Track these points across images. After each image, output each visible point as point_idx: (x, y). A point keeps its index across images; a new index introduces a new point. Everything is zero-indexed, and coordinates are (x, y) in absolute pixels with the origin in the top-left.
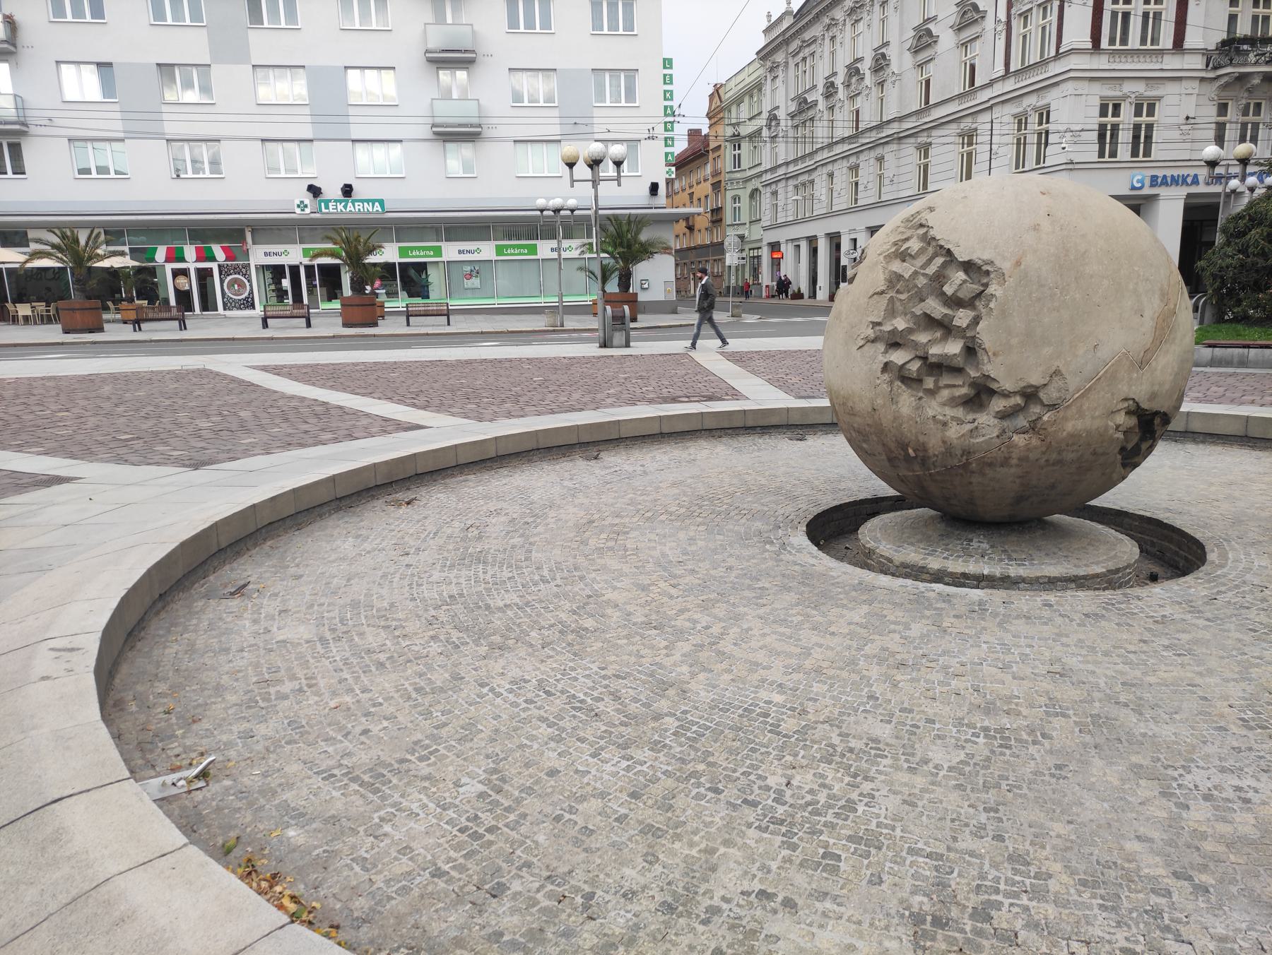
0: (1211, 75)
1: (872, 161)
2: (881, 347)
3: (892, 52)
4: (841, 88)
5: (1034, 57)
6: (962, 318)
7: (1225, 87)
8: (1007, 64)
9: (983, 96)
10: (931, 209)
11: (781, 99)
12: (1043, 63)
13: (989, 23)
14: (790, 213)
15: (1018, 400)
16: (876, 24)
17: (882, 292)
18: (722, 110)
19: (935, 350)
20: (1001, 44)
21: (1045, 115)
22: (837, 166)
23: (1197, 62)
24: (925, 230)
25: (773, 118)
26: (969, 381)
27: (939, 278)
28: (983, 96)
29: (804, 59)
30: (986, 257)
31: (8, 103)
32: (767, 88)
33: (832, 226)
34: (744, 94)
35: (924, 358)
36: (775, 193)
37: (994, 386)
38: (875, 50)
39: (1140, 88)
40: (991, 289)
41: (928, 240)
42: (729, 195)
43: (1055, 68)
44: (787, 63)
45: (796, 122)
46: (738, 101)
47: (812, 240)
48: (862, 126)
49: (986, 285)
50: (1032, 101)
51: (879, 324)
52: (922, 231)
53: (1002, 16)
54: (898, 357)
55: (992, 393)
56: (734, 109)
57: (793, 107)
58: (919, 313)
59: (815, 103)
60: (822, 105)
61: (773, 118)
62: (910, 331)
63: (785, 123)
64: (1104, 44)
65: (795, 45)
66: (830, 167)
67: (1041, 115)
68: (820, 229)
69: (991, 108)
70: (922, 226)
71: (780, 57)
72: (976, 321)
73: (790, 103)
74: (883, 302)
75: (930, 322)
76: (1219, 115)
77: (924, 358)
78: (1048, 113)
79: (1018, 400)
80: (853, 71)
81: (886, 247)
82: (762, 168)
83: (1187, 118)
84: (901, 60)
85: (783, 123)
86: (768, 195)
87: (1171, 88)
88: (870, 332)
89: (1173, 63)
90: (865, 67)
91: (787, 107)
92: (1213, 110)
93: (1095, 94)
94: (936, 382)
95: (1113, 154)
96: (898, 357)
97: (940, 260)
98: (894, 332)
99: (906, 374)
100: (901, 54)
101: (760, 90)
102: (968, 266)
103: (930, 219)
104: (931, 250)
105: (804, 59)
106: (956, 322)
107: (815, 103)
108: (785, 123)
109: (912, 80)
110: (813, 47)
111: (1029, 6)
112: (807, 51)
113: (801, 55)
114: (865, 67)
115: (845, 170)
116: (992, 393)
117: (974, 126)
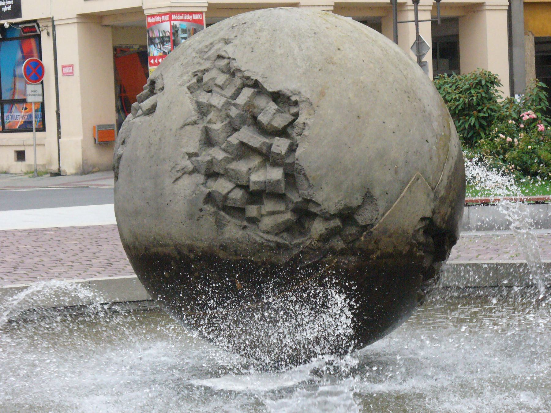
2: (199, 178)
6: (280, 145)
15: (337, 222)
19: (255, 177)
24: (226, 61)
26: (291, 206)
27: (249, 108)
31: (144, 395)
35: (245, 187)
37: (314, 209)
40: (301, 120)
49: (296, 115)
51: (196, 155)
54: (222, 186)
70: (219, 57)
72: (292, 149)
75: (245, 151)
77: (245, 187)
79: (337, 222)
88: (188, 164)
94: (259, 210)
99: (229, 203)
102: (277, 97)
104: (238, 82)
116: (313, 216)
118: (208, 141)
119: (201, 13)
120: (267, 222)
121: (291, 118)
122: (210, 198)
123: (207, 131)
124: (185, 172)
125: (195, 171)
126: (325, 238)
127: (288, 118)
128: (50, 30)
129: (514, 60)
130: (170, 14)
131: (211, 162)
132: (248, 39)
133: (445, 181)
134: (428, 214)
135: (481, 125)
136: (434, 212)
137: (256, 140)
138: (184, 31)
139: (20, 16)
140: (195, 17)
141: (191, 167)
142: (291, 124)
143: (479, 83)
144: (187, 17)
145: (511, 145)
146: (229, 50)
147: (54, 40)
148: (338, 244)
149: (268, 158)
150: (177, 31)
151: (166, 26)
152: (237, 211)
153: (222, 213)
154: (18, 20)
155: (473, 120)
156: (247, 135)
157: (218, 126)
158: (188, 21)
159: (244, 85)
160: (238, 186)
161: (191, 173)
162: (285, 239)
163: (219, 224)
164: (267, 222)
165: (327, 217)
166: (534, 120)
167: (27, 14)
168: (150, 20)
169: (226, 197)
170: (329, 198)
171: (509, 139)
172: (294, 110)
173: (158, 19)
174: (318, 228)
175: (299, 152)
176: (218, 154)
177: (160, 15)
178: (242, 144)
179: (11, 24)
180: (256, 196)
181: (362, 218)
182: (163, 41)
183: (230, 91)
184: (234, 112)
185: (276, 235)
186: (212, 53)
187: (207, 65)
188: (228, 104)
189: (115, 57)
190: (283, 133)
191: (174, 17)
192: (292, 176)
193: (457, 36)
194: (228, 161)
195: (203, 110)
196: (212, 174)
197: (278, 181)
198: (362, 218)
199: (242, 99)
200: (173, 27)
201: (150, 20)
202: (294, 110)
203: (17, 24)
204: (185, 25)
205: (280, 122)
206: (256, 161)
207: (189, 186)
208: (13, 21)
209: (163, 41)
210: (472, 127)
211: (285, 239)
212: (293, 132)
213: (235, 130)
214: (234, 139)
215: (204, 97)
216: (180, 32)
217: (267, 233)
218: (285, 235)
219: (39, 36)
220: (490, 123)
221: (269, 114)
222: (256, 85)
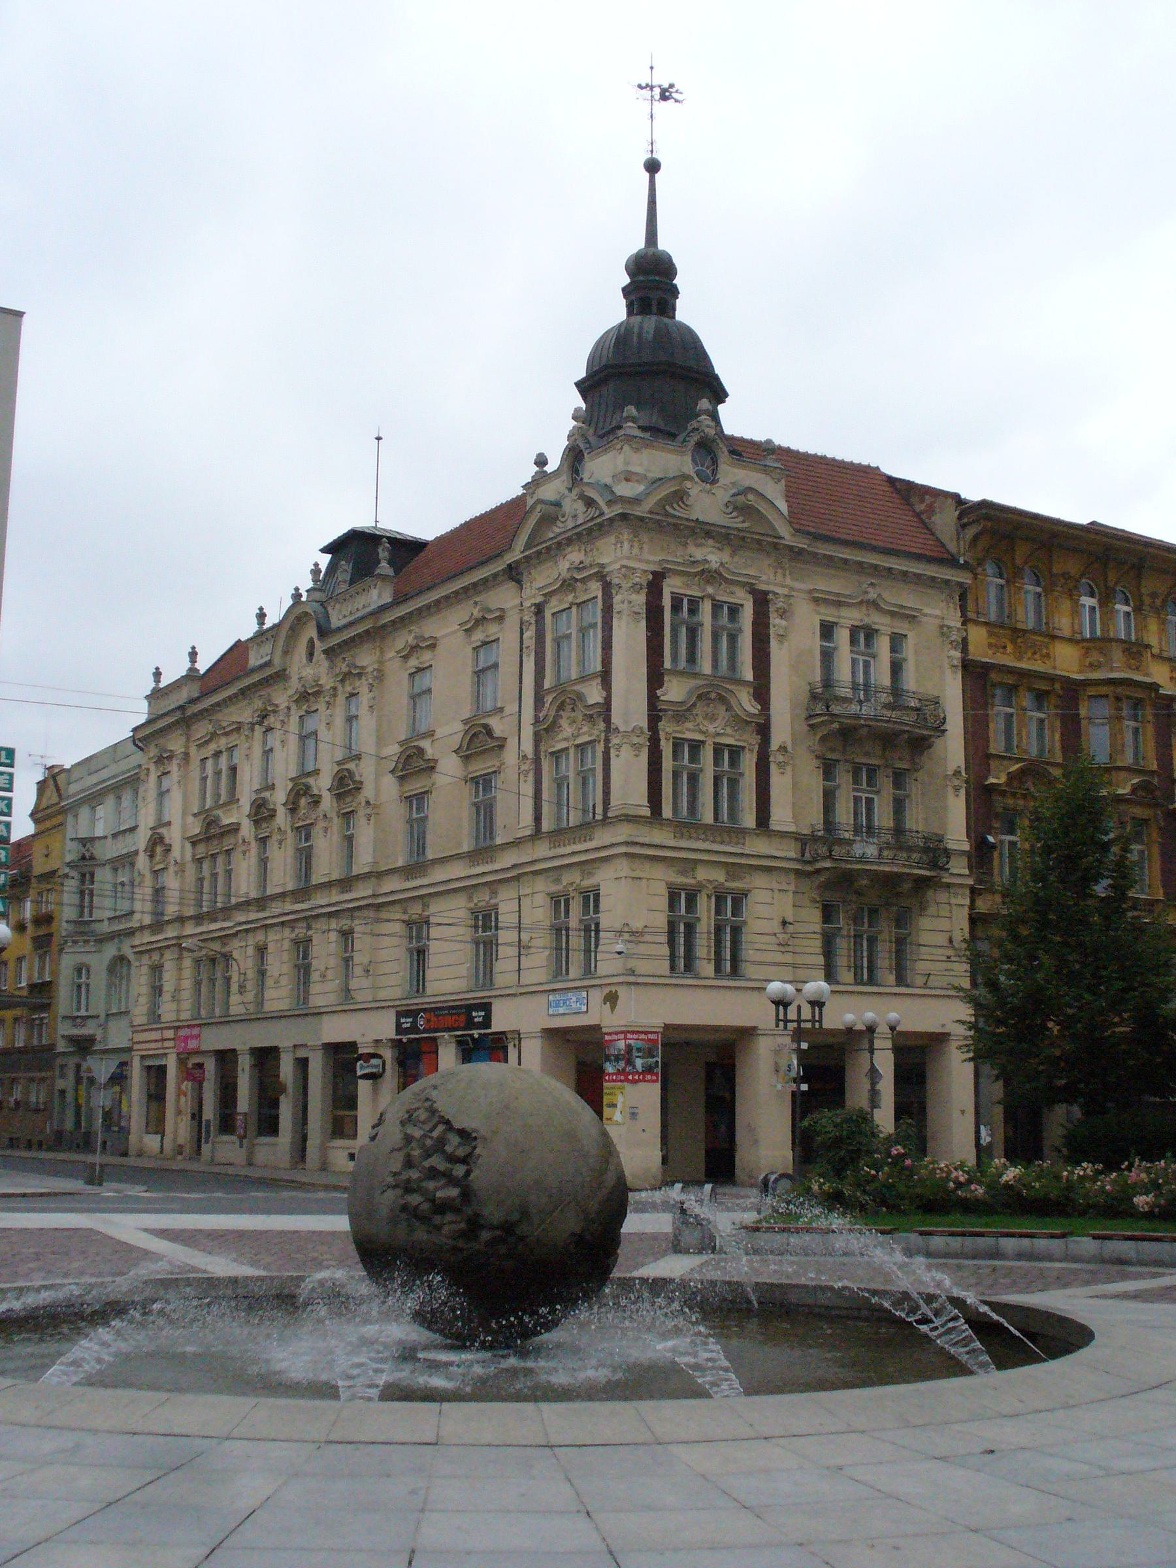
0: (809, 868)
1: (333, 936)
2: (399, 1192)
3: (366, 771)
4: (281, 812)
5: (574, 819)
6: (459, 1170)
8: (538, 818)
10: (435, 1087)
11: (174, 808)
13: (510, 756)
15: (498, 1233)
16: (339, 721)
17: (400, 1149)
18: (63, 811)
19: (439, 1194)
20: (528, 789)
22: (273, 936)
23: (789, 850)
25: (157, 842)
27: (442, 1141)
28: (507, 860)
29: (218, 754)
30: (473, 1126)
33: (262, 1036)
36: (157, 969)
38: (339, 763)
39: (719, 876)
40: (477, 1151)
41: (433, 1111)
42: (68, 962)
43: (603, 837)
45: (201, 850)
46: (93, 799)
47: (226, 1057)
48: (316, 879)
49: (475, 1148)
50: (573, 878)
52: (427, 1104)
53: (528, 747)
54: (415, 1199)
55: (482, 1227)
56: (84, 812)
57: (196, 829)
61: (157, 842)
62: (420, 1180)
64: (667, 812)
66: (260, 937)
68: (243, 1039)
69: (518, 878)
70: (427, 1099)
71: (175, 744)
74: (400, 1157)
75: (433, 1173)
76: (825, 922)
77: (433, 1201)
81: (401, 1114)
82: (134, 924)
83: (784, 923)
84: (381, 786)
85: (176, 853)
86: (145, 970)
87: (759, 881)
88: (390, 1180)
89: (760, 846)
91: (184, 827)
93: (659, 879)
97: (441, 1128)
100: (378, 776)
102: (463, 1133)
104: (435, 1120)
105: (218, 754)
107: (235, 829)
109: (395, 813)
110: (233, 739)
111: (563, 745)
112: (223, 742)
113: (213, 747)
114: (323, 784)
115: (287, 945)
116: (482, 1227)
117: (493, 901)
118: (409, 1163)
122: (405, 1208)
123: (408, 1155)
125: (396, 1186)
127: (467, 1149)
131: (408, 1181)
134: (578, 1229)
138: (639, 1050)
139: (490, 1027)
142: (470, 1155)
144: (643, 1036)
146: (434, 1094)
149: (451, 1180)
151: (621, 1044)
152: (424, 1219)
154: (489, 1031)
155: (842, 1153)
156: (436, 1161)
159: (439, 1122)
160: (427, 1200)
162: (461, 1243)
164: (446, 1230)
165: (492, 1228)
166: (903, 1155)
167: (496, 1027)
168: (607, 1038)
169: (416, 1207)
170: (492, 1213)
171: (873, 1172)
172: (474, 1144)
173: (615, 1037)
174: (485, 1235)
176: (414, 1174)
177: (616, 1033)
180: (441, 1207)
182: (617, 1058)
183: (427, 1127)
184: (429, 1142)
186: (423, 1096)
187: (417, 1105)
190: (464, 1160)
191: (629, 1036)
195: (408, 1139)
196: (408, 1188)
199: (435, 1134)
204: (640, 1044)
205: (461, 1152)
206: (442, 1182)
208: (482, 1031)
209: (617, 1058)
210: (842, 1159)
211: (461, 1243)
213: (429, 1156)
214: (426, 1164)
221: (453, 1144)
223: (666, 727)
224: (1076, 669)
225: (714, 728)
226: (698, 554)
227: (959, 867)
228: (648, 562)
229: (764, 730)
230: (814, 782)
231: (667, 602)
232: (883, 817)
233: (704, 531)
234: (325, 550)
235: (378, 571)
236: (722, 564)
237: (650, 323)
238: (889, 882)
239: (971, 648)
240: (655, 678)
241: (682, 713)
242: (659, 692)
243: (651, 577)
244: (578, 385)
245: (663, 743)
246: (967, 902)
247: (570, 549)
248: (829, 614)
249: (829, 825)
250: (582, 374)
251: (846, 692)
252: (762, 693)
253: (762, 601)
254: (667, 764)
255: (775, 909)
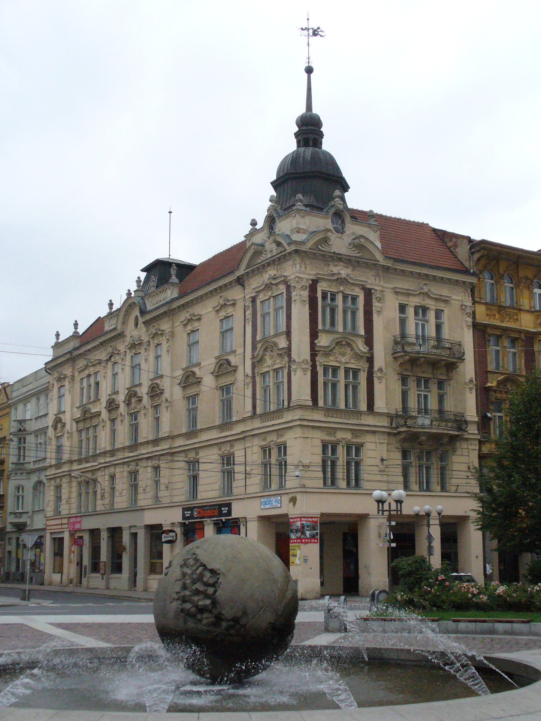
1: (149, 469)
2: (179, 602)
3: (165, 384)
4: (122, 406)
6: (211, 590)
7: (404, 440)
9: (239, 429)
10: (198, 547)
11: (67, 405)
12: (279, 412)
13: (240, 375)
14: (74, 506)
15: (232, 623)
17: (180, 580)
18: (10, 406)
19: (200, 603)
21: (282, 448)
22: (118, 469)
23: (384, 422)
27: (201, 575)
28: (239, 429)
29: (89, 376)
32: (54, 393)
33: (114, 522)
34: (32, 395)
39: (348, 436)
40: (219, 581)
41: (196, 560)
44: (73, 376)
45: (81, 425)
47: (94, 533)
49: (218, 579)
51: (179, 593)
54: (188, 606)
58: (194, 588)
59: (99, 414)
60: (105, 415)
61: (58, 421)
63: (70, 426)
64: (321, 403)
65: (81, 363)
66: (112, 470)
67: (280, 449)
68: (103, 523)
69: (244, 438)
70: (194, 554)
72: (215, 591)
73: (75, 410)
74: (180, 584)
75: (197, 592)
77: (197, 606)
78: (285, 448)
80: (132, 395)
85: (68, 427)
86: (52, 488)
88: (176, 596)
89: (369, 420)
90: (143, 391)
92: (399, 455)
95: (333, 483)
96: (188, 606)
97: (201, 569)
98: (184, 596)
100: (172, 386)
101: (47, 395)
102: (212, 571)
103: (198, 551)
104: (198, 564)
105: (89, 376)
106: (208, 592)
107: (99, 414)
108: (70, 426)
109: (181, 406)
110: (98, 368)
112: (92, 370)
113: (87, 372)
114: (143, 391)
115: (125, 474)
116: (222, 620)
118: (184, 587)
119: (317, 517)
120: (205, 621)
121: (216, 580)
122: (182, 610)
124: (174, 599)
126: (228, 628)
127: (215, 579)
128: (245, 523)
129: (482, 548)
130: (301, 518)
132: (205, 547)
133: (282, 609)
134: (273, 621)
135: (417, 582)
136: (275, 621)
137: (201, 588)
138: (308, 527)
140: (314, 519)
141: (176, 597)
142: (216, 582)
143: (417, 561)
144: (310, 520)
145: (430, 592)
147: (246, 527)
148: (233, 632)
149: (207, 596)
150: (304, 527)
151: (299, 524)
152: (193, 616)
153: (187, 617)
154: (230, 518)
156: (199, 586)
157: (188, 582)
158: (310, 521)
161: (177, 600)
163: (185, 622)
164: (205, 621)
167: (234, 515)
168: (291, 520)
170: (228, 612)
171: (429, 589)
172: (218, 577)
173: (295, 520)
174: (224, 624)
175: (217, 593)
176: (187, 593)
177: (296, 518)
178: (197, 589)
179: (226, 519)
180: (202, 610)
181: (243, 621)
185: (208, 626)
187: (189, 557)
188: (193, 573)
189: (277, 538)
190: (213, 585)
191: (302, 519)
192: (214, 603)
193: (456, 532)
194: (191, 596)
195: (184, 575)
197: (208, 605)
198: (243, 621)
199: (198, 572)
200: (302, 524)
201: (291, 520)
202: (218, 577)
203: (229, 520)
204: (308, 523)
205: (212, 581)
206: (202, 597)
207: (175, 605)
209: (297, 531)
211: (211, 628)
212: (217, 585)
213: (195, 583)
214: (194, 587)
215: (186, 570)
216: (305, 527)
217: (205, 625)
218: (212, 627)
219: (240, 526)
220: (421, 581)
222: (204, 565)
223: (319, 359)
224: (532, 326)
225: (344, 359)
226: (335, 270)
227: (473, 429)
228: (309, 274)
229: (370, 360)
230: (397, 387)
231: (319, 295)
232: (433, 404)
233: (338, 258)
234: (143, 270)
235: (171, 281)
236: (348, 275)
237: (309, 151)
238: (436, 438)
239: (477, 316)
240: (314, 334)
241: (328, 352)
242: (316, 341)
243: (311, 282)
244: (272, 183)
245: (318, 367)
246: (477, 448)
247: (269, 268)
248: (403, 300)
249: (405, 408)
250: (274, 178)
251: (412, 340)
252: (369, 341)
253: (368, 294)
254: (321, 379)
255: (377, 452)
